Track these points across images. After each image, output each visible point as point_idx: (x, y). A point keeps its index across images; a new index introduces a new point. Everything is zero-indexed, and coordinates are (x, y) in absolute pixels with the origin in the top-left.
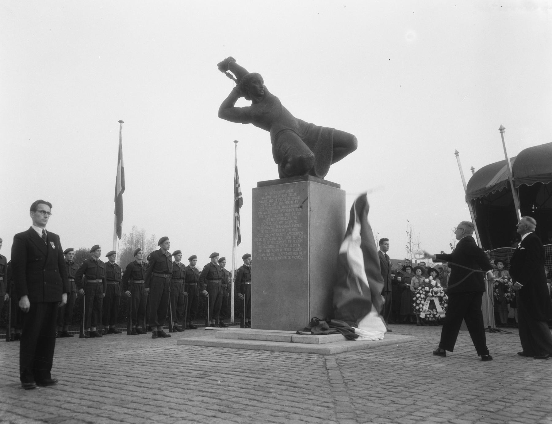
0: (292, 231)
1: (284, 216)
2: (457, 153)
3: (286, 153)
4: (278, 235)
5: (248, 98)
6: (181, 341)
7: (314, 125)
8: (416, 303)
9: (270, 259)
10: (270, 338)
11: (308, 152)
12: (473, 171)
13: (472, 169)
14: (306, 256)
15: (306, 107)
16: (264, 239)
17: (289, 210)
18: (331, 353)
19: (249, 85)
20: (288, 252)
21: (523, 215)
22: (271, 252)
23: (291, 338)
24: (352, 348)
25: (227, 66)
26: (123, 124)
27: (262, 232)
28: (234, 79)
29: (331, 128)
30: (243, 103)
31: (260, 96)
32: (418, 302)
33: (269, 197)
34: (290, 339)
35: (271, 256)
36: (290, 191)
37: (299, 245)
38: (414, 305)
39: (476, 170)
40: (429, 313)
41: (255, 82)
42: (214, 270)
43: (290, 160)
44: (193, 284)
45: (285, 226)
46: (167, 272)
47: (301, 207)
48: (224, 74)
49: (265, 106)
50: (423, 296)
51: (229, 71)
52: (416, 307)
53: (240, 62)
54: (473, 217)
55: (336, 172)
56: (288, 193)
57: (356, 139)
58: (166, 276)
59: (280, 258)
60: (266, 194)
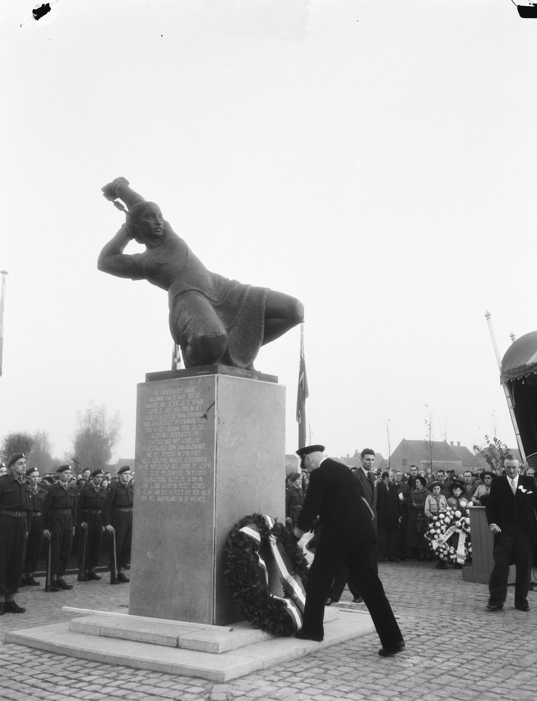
0: (191, 456)
1: (181, 431)
2: (488, 316)
3: (185, 329)
4: (171, 460)
5: (140, 240)
6: (11, 636)
7: (237, 283)
8: (434, 525)
9: (159, 499)
10: (145, 638)
11: (229, 329)
12: (513, 339)
13: (512, 336)
14: (210, 498)
15: (227, 252)
16: (152, 466)
17: (188, 421)
18: (226, 680)
19: (144, 222)
20: (185, 490)
21: (495, 529)
22: (160, 489)
23: (178, 640)
24: (273, 662)
25: (116, 191)
26: (6, 276)
27: (149, 455)
28: (125, 211)
29: (264, 288)
30: (134, 248)
31: (157, 237)
32: (438, 524)
33: (160, 399)
34: (175, 641)
35: (161, 495)
36: (190, 390)
37: (201, 478)
38: (431, 525)
39: (517, 338)
40: (444, 547)
41: (147, 216)
42: (123, 492)
43: (189, 340)
44: (94, 512)
45: (182, 448)
46: (20, 509)
47: (205, 416)
48: (111, 203)
49: (163, 253)
50: (447, 520)
51: (119, 200)
52: (431, 529)
53: (135, 187)
54: (511, 404)
55: (273, 357)
56: (187, 394)
57: (301, 305)
58: (18, 514)
59: (173, 499)
60: (156, 393)
